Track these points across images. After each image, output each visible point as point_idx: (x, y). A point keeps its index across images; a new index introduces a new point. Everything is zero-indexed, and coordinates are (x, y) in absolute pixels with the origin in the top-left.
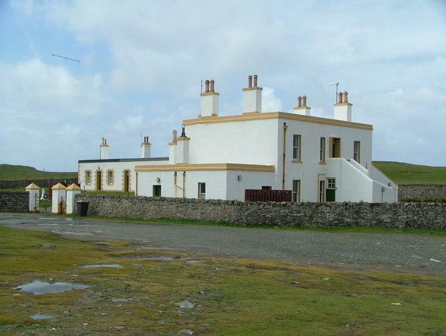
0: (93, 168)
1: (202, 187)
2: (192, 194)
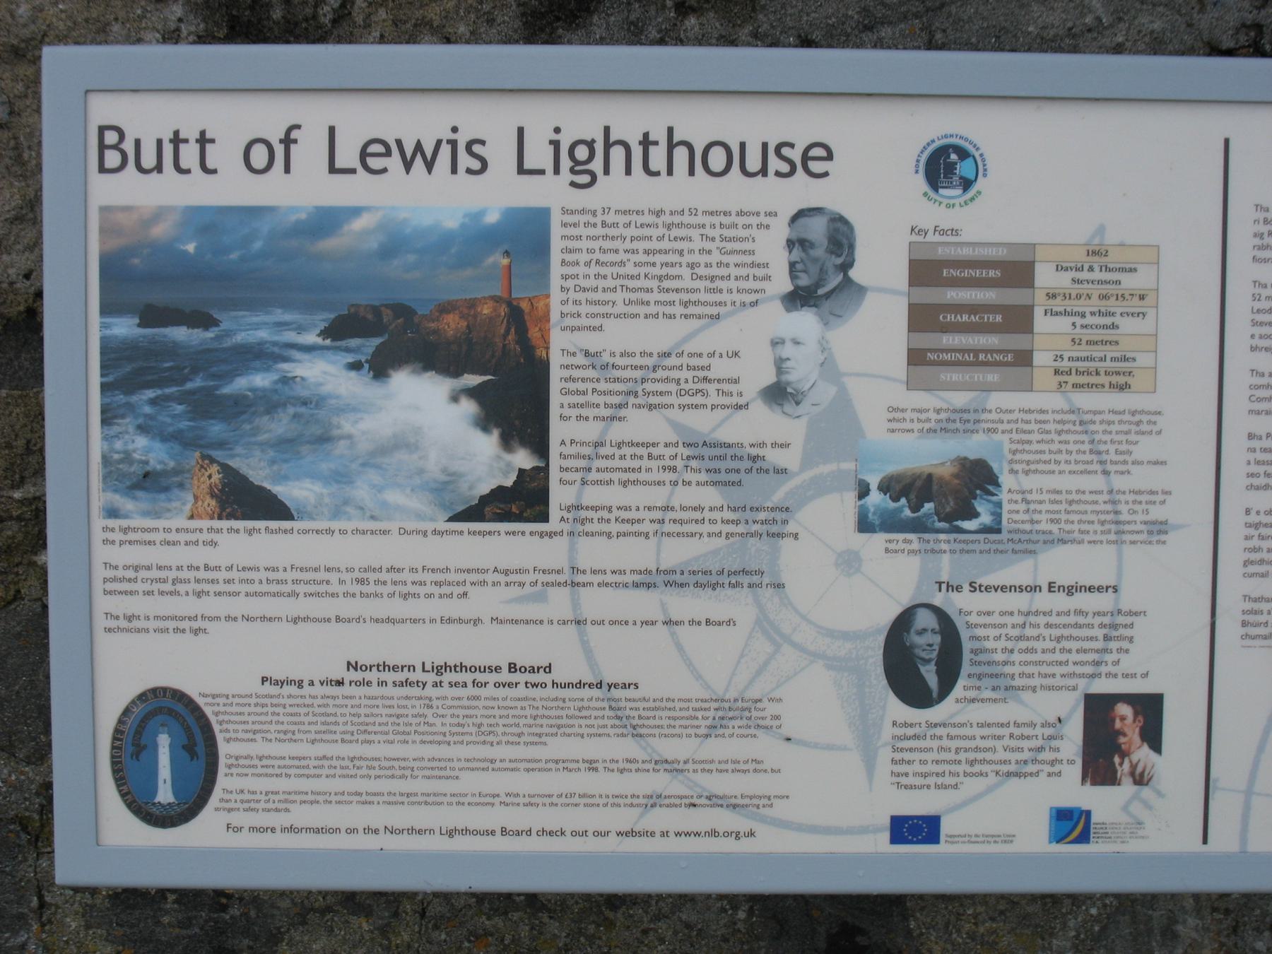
1: (656, 143)
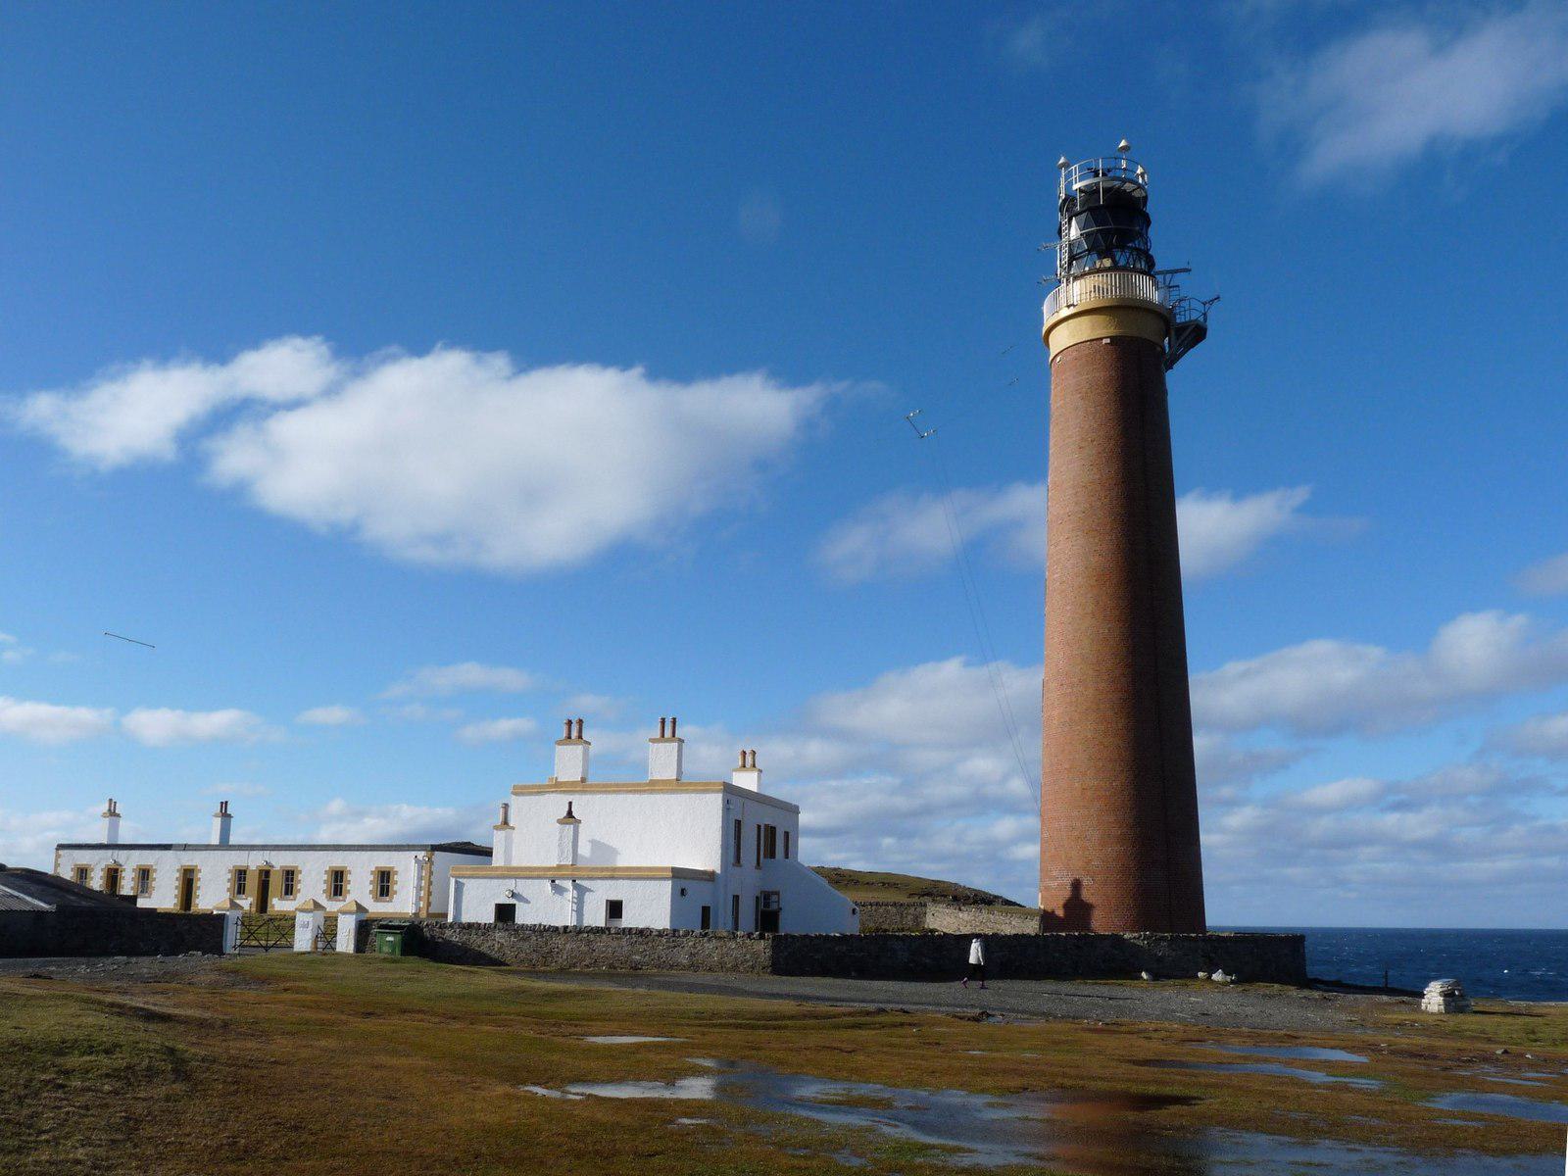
0: (105, 859)
2: (596, 917)
